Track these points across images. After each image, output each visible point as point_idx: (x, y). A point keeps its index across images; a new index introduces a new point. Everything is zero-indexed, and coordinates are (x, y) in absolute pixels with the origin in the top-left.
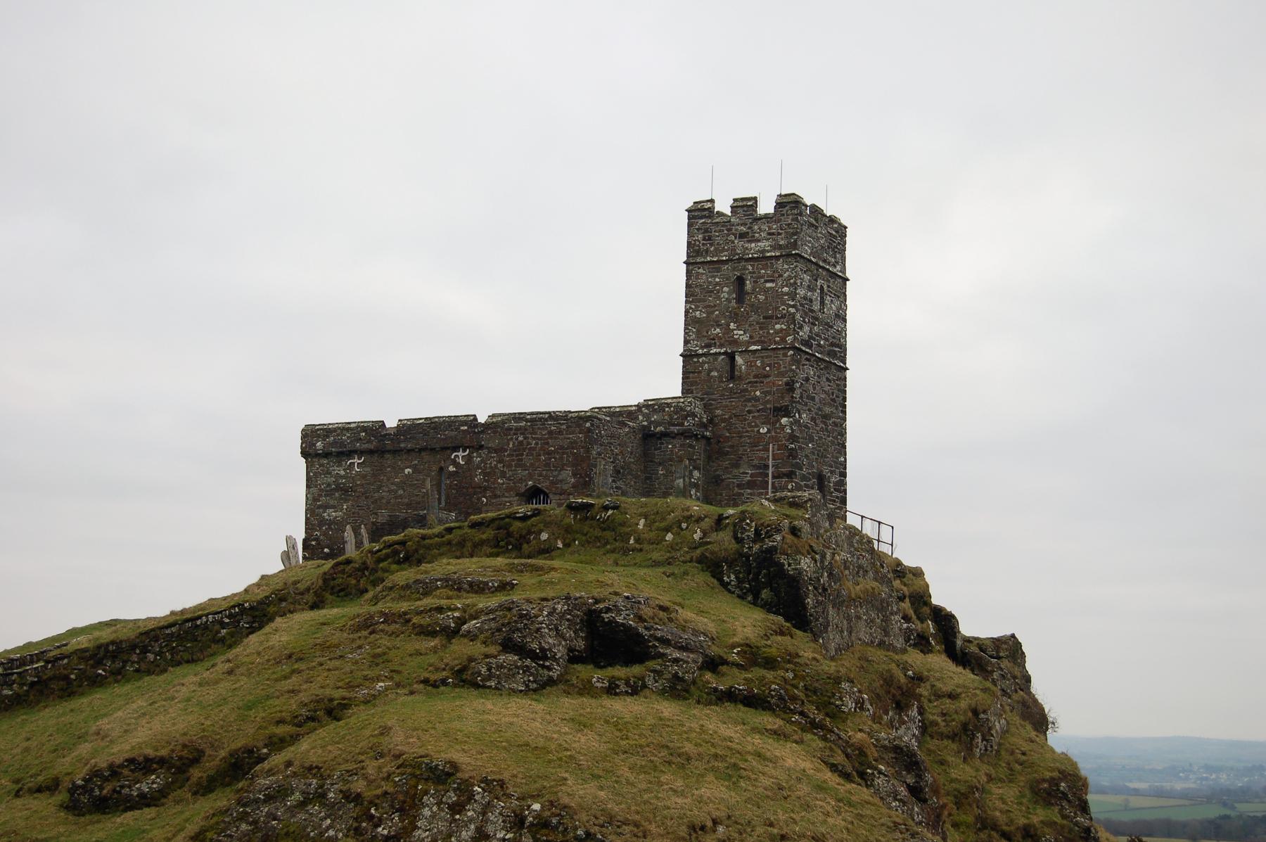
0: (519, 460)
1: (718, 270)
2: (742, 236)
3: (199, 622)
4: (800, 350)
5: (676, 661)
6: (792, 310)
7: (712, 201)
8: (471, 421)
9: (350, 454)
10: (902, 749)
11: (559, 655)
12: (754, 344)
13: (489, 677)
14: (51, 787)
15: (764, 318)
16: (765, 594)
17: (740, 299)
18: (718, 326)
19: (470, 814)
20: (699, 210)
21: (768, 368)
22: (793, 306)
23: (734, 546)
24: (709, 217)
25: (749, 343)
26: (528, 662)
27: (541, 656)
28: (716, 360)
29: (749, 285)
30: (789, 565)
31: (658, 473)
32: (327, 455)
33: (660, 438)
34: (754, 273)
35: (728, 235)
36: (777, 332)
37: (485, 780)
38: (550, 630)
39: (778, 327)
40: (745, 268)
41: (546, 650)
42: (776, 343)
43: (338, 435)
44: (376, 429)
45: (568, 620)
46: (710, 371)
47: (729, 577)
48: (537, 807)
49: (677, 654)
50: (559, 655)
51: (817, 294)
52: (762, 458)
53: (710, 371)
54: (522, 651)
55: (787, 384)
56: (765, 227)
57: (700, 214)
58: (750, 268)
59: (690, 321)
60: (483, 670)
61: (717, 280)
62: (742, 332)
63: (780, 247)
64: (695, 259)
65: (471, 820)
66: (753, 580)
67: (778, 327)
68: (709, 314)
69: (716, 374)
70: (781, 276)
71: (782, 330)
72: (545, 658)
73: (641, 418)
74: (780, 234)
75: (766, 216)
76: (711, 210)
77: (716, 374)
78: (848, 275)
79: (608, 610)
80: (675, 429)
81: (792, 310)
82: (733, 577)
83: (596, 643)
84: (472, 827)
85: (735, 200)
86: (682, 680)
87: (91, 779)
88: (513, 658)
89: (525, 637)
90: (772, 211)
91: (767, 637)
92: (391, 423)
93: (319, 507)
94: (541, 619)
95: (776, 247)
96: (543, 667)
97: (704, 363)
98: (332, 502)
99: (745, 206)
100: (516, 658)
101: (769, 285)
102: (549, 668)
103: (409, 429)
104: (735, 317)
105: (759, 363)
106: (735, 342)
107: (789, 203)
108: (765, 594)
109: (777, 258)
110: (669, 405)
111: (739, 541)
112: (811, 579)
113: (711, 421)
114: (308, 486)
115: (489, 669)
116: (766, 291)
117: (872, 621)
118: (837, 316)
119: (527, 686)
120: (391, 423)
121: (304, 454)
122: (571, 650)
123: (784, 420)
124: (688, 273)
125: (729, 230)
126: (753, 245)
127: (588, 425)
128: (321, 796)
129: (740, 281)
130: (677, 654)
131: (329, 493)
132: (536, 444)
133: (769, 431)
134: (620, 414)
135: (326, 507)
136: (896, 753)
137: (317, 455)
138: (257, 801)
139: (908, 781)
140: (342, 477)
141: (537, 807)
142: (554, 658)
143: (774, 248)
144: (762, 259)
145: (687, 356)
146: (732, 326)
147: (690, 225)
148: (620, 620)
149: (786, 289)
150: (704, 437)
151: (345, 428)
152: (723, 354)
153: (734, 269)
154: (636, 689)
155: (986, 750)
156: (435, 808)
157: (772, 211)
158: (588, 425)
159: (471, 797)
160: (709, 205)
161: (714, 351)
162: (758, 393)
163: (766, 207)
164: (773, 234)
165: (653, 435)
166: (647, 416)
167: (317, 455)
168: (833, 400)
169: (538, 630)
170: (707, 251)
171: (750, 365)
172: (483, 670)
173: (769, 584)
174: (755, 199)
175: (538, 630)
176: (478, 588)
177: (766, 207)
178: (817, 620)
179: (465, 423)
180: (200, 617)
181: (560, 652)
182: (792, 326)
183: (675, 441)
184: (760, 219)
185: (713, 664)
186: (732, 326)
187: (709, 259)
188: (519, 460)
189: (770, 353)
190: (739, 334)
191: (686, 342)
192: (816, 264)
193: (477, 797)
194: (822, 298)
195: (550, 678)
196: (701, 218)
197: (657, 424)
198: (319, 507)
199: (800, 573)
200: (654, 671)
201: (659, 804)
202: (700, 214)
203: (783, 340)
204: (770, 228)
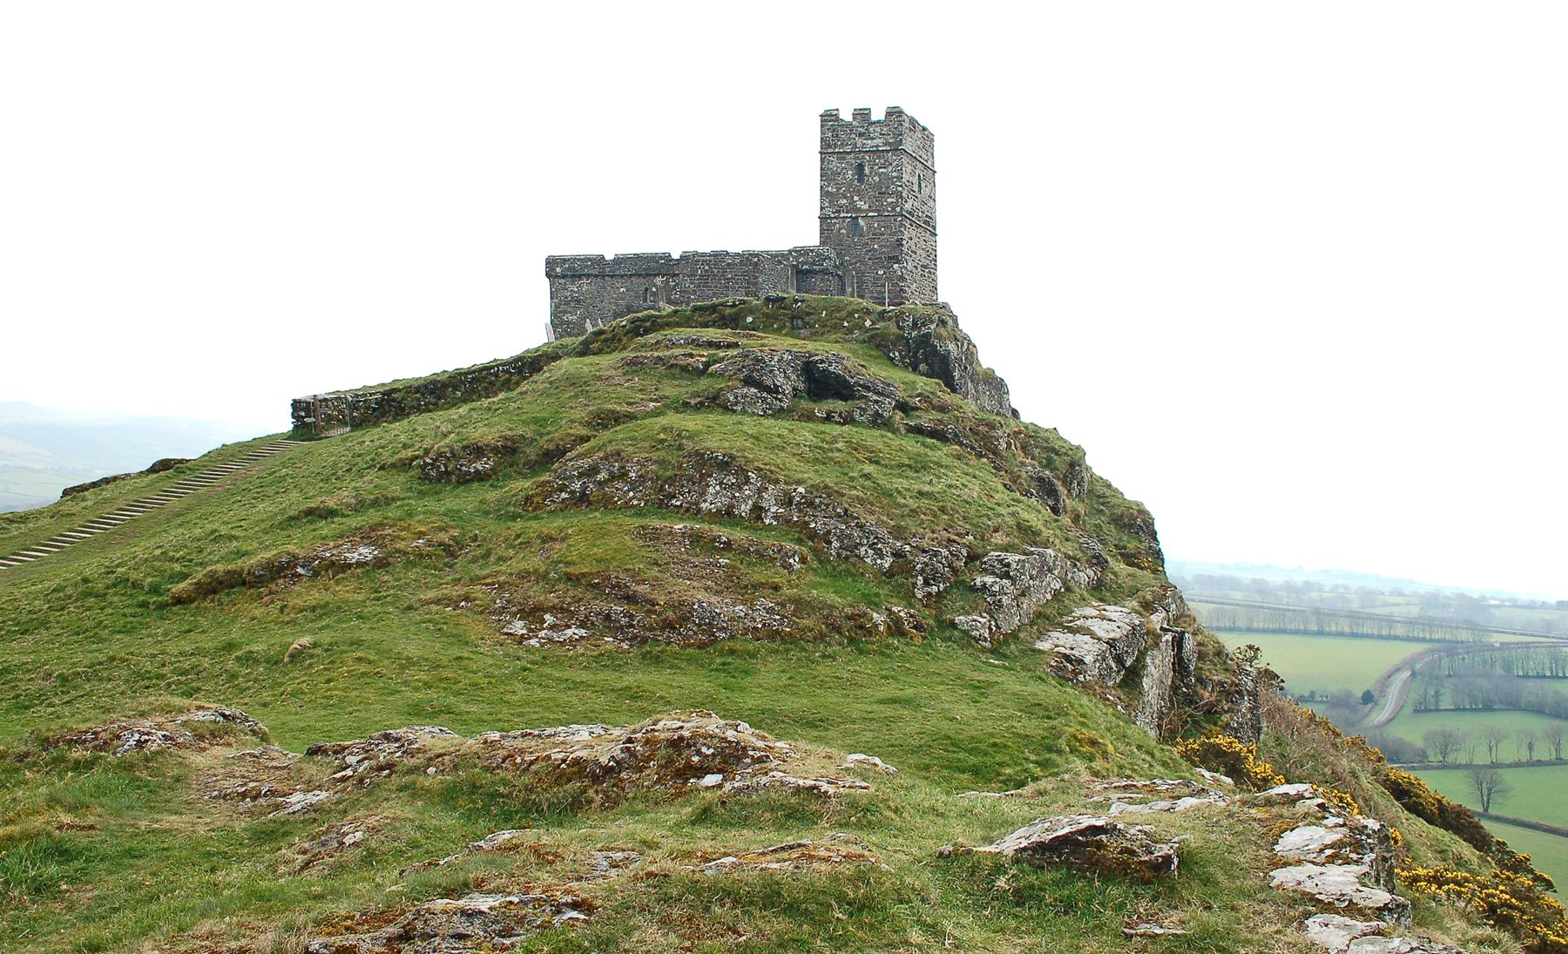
0: (706, 283)
1: (844, 159)
2: (861, 135)
3: (492, 371)
4: (906, 217)
5: (876, 402)
6: (900, 189)
8: (667, 257)
9: (580, 277)
10: (1044, 479)
11: (787, 392)
12: (871, 211)
13: (736, 404)
14: (405, 465)
15: (879, 193)
16: (922, 367)
17: (861, 180)
18: (845, 198)
19: (747, 492)
20: (828, 115)
21: (883, 229)
22: (901, 186)
24: (837, 121)
25: (869, 211)
26: (765, 395)
27: (774, 390)
28: (844, 222)
29: (867, 171)
30: (941, 347)
32: (564, 277)
33: (805, 274)
34: (870, 161)
35: (851, 134)
36: (889, 204)
37: (759, 469)
38: (780, 372)
39: (889, 200)
40: (863, 158)
41: (778, 386)
42: (888, 211)
43: (572, 263)
44: (599, 260)
45: (792, 367)
46: (840, 229)
47: (894, 354)
48: (801, 490)
49: (875, 397)
50: (787, 392)
51: (916, 180)
52: (880, 292)
53: (840, 229)
54: (760, 385)
55: (897, 240)
56: (878, 129)
57: (829, 119)
58: (868, 158)
59: (824, 194)
60: (732, 398)
61: (843, 165)
62: (863, 203)
64: (827, 149)
65: (749, 497)
66: (912, 357)
67: (889, 200)
68: (838, 189)
69: (845, 232)
70: (891, 164)
71: (892, 202)
72: (778, 393)
73: (791, 259)
74: (889, 135)
75: (879, 122)
77: (845, 232)
79: (822, 361)
80: (817, 268)
81: (900, 189)
82: (897, 354)
83: (812, 386)
84: (750, 502)
85: (855, 110)
86: (882, 416)
87: (437, 459)
88: (753, 390)
89: (762, 376)
92: (609, 257)
93: (560, 312)
94: (773, 363)
96: (776, 399)
97: (835, 223)
98: (569, 309)
99: (862, 115)
100: (756, 391)
101: (881, 170)
102: (781, 400)
103: (619, 261)
105: (876, 225)
106: (859, 210)
107: (895, 113)
108: (922, 367)
109: (888, 151)
110: (812, 251)
112: (956, 358)
113: (842, 264)
114: (551, 298)
115: (736, 397)
116: (880, 175)
117: (993, 396)
119: (765, 412)
121: (548, 275)
122: (795, 389)
123: (896, 266)
124: (822, 160)
126: (869, 141)
127: (756, 260)
128: (623, 475)
129: (860, 167)
130: (875, 397)
131: (567, 303)
132: (718, 272)
133: (885, 273)
134: (777, 256)
135: (565, 312)
136: (1039, 482)
137: (557, 277)
138: (572, 477)
139: (1049, 503)
140: (575, 292)
141: (801, 490)
143: (885, 144)
144: (876, 152)
145: (823, 219)
146: (856, 198)
147: (822, 126)
148: (831, 369)
149: (895, 174)
150: (837, 275)
151: (575, 259)
152: (850, 217)
153: (856, 158)
154: (848, 420)
155: (1080, 492)
156: (718, 488)
157: (884, 119)
158: (756, 260)
159: (747, 481)
160: (836, 112)
161: (842, 215)
162: (876, 246)
163: (878, 115)
164: (884, 134)
165: (801, 271)
166: (796, 258)
167: (557, 277)
168: (928, 256)
169: (771, 371)
171: (870, 227)
172: (732, 398)
173: (925, 360)
175: (771, 371)
176: (718, 346)
177: (878, 115)
178: (961, 389)
179: (661, 258)
180: (493, 367)
181: (788, 389)
182: (900, 200)
183: (817, 277)
184: (874, 123)
185: (903, 407)
186: (856, 198)
187: (837, 150)
188: (706, 283)
189: (884, 218)
190: (860, 204)
191: (822, 208)
192: (915, 158)
193: (751, 481)
194: (919, 183)
195: (782, 408)
196: (830, 121)
197: (804, 263)
198: (560, 312)
199: (949, 353)
200: (860, 408)
202: (829, 119)
203: (894, 209)
204: (882, 130)
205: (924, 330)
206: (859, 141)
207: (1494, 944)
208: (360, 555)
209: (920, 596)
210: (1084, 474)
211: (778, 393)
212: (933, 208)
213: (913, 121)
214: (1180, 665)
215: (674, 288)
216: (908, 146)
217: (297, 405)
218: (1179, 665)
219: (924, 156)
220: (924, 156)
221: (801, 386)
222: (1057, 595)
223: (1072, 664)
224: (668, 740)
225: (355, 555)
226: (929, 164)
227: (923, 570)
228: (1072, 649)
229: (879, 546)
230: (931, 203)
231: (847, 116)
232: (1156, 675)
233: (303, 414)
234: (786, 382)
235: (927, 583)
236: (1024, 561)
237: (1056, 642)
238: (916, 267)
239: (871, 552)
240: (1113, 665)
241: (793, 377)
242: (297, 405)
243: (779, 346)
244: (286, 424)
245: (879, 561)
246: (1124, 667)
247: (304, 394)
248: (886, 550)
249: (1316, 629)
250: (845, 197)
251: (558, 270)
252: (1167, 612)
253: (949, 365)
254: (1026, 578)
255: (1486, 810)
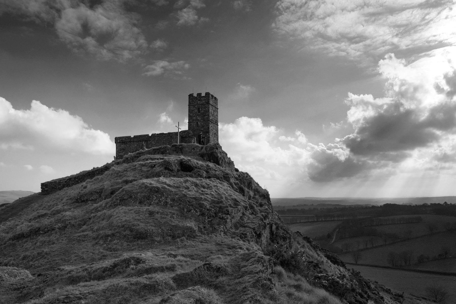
2: (199, 100)
7: (193, 94)
16: (212, 161)
17: (199, 112)
23: (206, 152)
29: (200, 110)
31: (203, 132)
32: (120, 143)
44: (129, 138)
48: (177, 196)
51: (213, 112)
56: (203, 99)
57: (191, 96)
63: (206, 102)
65: (163, 200)
67: (206, 117)
75: (204, 96)
76: (193, 95)
78: (218, 108)
79: (185, 162)
90: (204, 95)
91: (396, 82)
95: (206, 102)
96: (173, 173)
98: (121, 152)
99: (199, 95)
102: (174, 173)
104: (198, 115)
106: (198, 120)
107: (208, 94)
108: (212, 161)
111: (207, 151)
118: (217, 115)
120: (132, 136)
122: (178, 170)
125: (197, 99)
127: (171, 135)
129: (199, 109)
135: (120, 153)
142: (175, 171)
144: (203, 104)
163: (203, 95)
170: (193, 103)
174: (201, 93)
177: (203, 95)
181: (176, 170)
186: (198, 117)
190: (199, 118)
195: (174, 175)
197: (184, 135)
201: (15, 262)
202: (191, 96)
203: (207, 119)
205: (212, 151)
206: (199, 102)
207: (397, 303)
208: (58, 226)
209: (206, 222)
210: (253, 185)
211: (173, 171)
212: (217, 119)
213: (212, 96)
214: (272, 233)
215: (150, 144)
216: (211, 102)
217: (43, 185)
218: (272, 232)
219: (215, 105)
220: (215, 105)
221: (179, 169)
222: (241, 217)
223: (244, 235)
224: (341, 299)
225: (57, 226)
226: (216, 107)
227: (207, 215)
228: (244, 231)
229: (196, 209)
230: (217, 117)
231: (195, 95)
232: (265, 236)
233: (44, 187)
234: (176, 168)
235: (208, 218)
236: (233, 210)
237: (240, 230)
238: (213, 134)
239: (194, 211)
240: (254, 234)
241: (177, 166)
242: (43, 185)
243: (173, 158)
244: (38, 190)
245: (196, 214)
246: (257, 234)
247: (44, 181)
248: (198, 210)
249: (299, 222)
250: (195, 117)
251: (118, 141)
252: (269, 219)
253: (218, 160)
254: (233, 214)
255: (356, 263)
